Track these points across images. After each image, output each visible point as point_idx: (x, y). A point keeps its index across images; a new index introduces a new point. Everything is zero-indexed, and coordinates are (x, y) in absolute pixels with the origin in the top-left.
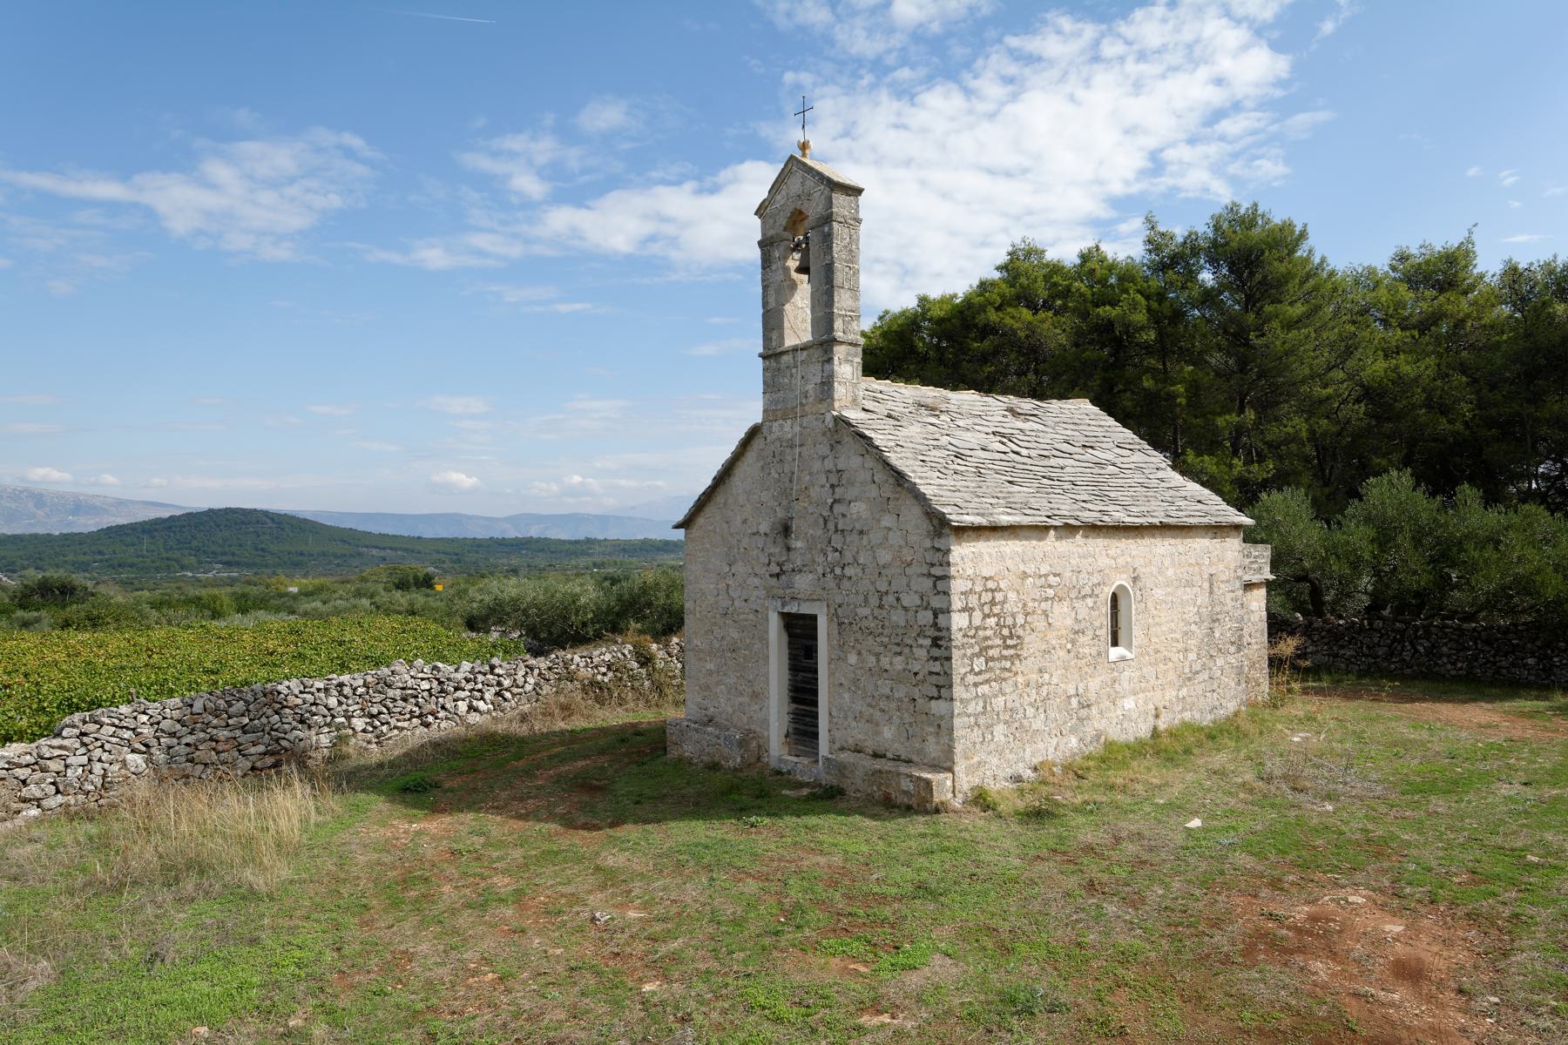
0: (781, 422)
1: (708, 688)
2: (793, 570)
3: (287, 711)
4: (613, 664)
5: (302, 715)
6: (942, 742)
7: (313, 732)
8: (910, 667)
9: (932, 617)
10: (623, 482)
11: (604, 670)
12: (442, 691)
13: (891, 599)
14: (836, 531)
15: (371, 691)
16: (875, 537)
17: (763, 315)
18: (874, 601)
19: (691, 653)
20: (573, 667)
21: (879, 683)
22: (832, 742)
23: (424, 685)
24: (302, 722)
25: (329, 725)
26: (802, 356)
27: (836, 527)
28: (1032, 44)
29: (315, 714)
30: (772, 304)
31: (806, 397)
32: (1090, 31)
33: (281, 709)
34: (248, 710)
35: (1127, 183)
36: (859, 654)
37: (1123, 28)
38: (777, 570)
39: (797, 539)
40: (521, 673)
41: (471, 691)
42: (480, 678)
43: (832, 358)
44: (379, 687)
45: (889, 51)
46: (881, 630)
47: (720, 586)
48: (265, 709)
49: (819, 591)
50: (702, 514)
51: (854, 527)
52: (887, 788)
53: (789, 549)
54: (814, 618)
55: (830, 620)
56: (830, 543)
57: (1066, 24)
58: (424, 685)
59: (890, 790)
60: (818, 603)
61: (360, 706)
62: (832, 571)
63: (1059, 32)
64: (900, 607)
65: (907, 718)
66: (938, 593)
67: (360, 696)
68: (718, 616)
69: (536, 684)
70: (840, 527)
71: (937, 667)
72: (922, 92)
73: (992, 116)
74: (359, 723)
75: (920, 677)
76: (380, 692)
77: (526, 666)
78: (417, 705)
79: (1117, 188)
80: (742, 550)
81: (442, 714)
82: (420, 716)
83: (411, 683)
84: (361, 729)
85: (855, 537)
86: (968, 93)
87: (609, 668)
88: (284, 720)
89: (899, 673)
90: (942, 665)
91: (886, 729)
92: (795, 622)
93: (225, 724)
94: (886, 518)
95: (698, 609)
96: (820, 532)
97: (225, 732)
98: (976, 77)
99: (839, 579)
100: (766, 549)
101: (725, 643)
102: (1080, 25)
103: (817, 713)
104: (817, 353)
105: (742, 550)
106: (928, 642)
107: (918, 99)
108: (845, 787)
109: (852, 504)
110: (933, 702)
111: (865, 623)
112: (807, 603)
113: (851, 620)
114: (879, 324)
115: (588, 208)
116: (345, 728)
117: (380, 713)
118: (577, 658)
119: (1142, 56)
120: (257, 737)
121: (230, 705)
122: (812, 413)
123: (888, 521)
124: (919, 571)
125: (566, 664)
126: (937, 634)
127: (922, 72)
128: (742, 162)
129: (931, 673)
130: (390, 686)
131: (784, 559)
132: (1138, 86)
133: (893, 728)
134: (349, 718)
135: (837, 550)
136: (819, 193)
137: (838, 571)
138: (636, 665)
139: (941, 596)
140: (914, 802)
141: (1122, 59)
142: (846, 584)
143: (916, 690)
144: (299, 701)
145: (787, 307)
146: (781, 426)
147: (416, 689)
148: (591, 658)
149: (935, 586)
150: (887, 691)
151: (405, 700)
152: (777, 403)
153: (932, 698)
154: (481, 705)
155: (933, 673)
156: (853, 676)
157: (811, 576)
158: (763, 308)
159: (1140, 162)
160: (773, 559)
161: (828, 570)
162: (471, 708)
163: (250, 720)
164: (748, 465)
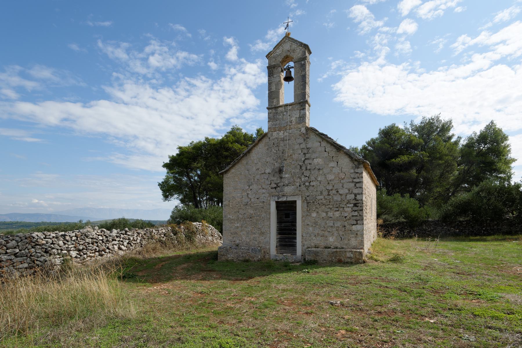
0: (278, 132)
2: (284, 185)
3: (38, 247)
4: (166, 234)
5: (46, 249)
6: (358, 239)
7: (52, 257)
8: (343, 215)
10: (55, 203)
11: (163, 236)
12: (107, 241)
13: (334, 192)
14: (306, 169)
15: (79, 239)
16: (325, 171)
23: (101, 238)
24: (46, 252)
25: (58, 254)
28: (194, 82)
29: (53, 249)
31: (291, 122)
32: (210, 82)
33: (35, 245)
34: (18, 246)
35: (220, 126)
36: (318, 212)
38: (275, 186)
39: (285, 174)
40: (136, 235)
41: (119, 241)
42: (122, 236)
43: (305, 108)
44: (82, 237)
45: (149, 73)
46: (328, 203)
47: (243, 194)
48: (27, 245)
49: (297, 192)
50: (234, 168)
51: (316, 168)
53: (281, 178)
54: (295, 202)
55: (303, 202)
57: (204, 78)
58: (101, 238)
59: (342, 258)
60: (297, 196)
61: (74, 246)
62: (304, 184)
63: (201, 80)
64: (338, 194)
65: (341, 233)
66: (357, 188)
67: (74, 241)
69: (141, 240)
70: (308, 168)
71: (356, 214)
72: (160, 89)
74: (74, 254)
75: (348, 217)
76: (83, 240)
77: (137, 233)
78: (97, 246)
79: (218, 127)
81: (107, 251)
82: (99, 251)
83: (95, 236)
84: (74, 256)
85: (316, 171)
86: (175, 92)
87: (164, 235)
88: (37, 251)
89: (337, 217)
91: (330, 238)
93: (4, 252)
94: (332, 163)
95: (231, 204)
96: (298, 171)
97: (6, 257)
99: (307, 187)
101: (246, 215)
103: (296, 237)
104: (298, 106)
105: (256, 180)
106: (352, 205)
107: (159, 90)
108: (318, 259)
110: (353, 226)
111: (320, 201)
114: (190, 145)
115: (38, 105)
116: (66, 256)
117: (83, 249)
118: (154, 231)
120: (24, 259)
121: (8, 243)
122: (294, 128)
124: (348, 181)
126: (356, 202)
128: (100, 100)
129: (353, 216)
130: (87, 237)
131: (279, 181)
133: (334, 237)
134: (69, 251)
135: (307, 176)
136: (299, 50)
137: (307, 184)
138: (172, 235)
139: (359, 189)
140: (353, 260)
141: (219, 90)
142: (311, 188)
143: (346, 223)
144: (44, 242)
146: (278, 134)
147: (97, 239)
150: (332, 224)
151: (93, 244)
154: (122, 247)
156: (314, 221)
157: (293, 187)
158: (269, 90)
159: (223, 121)
161: (302, 184)
162: (120, 249)
163: (20, 250)
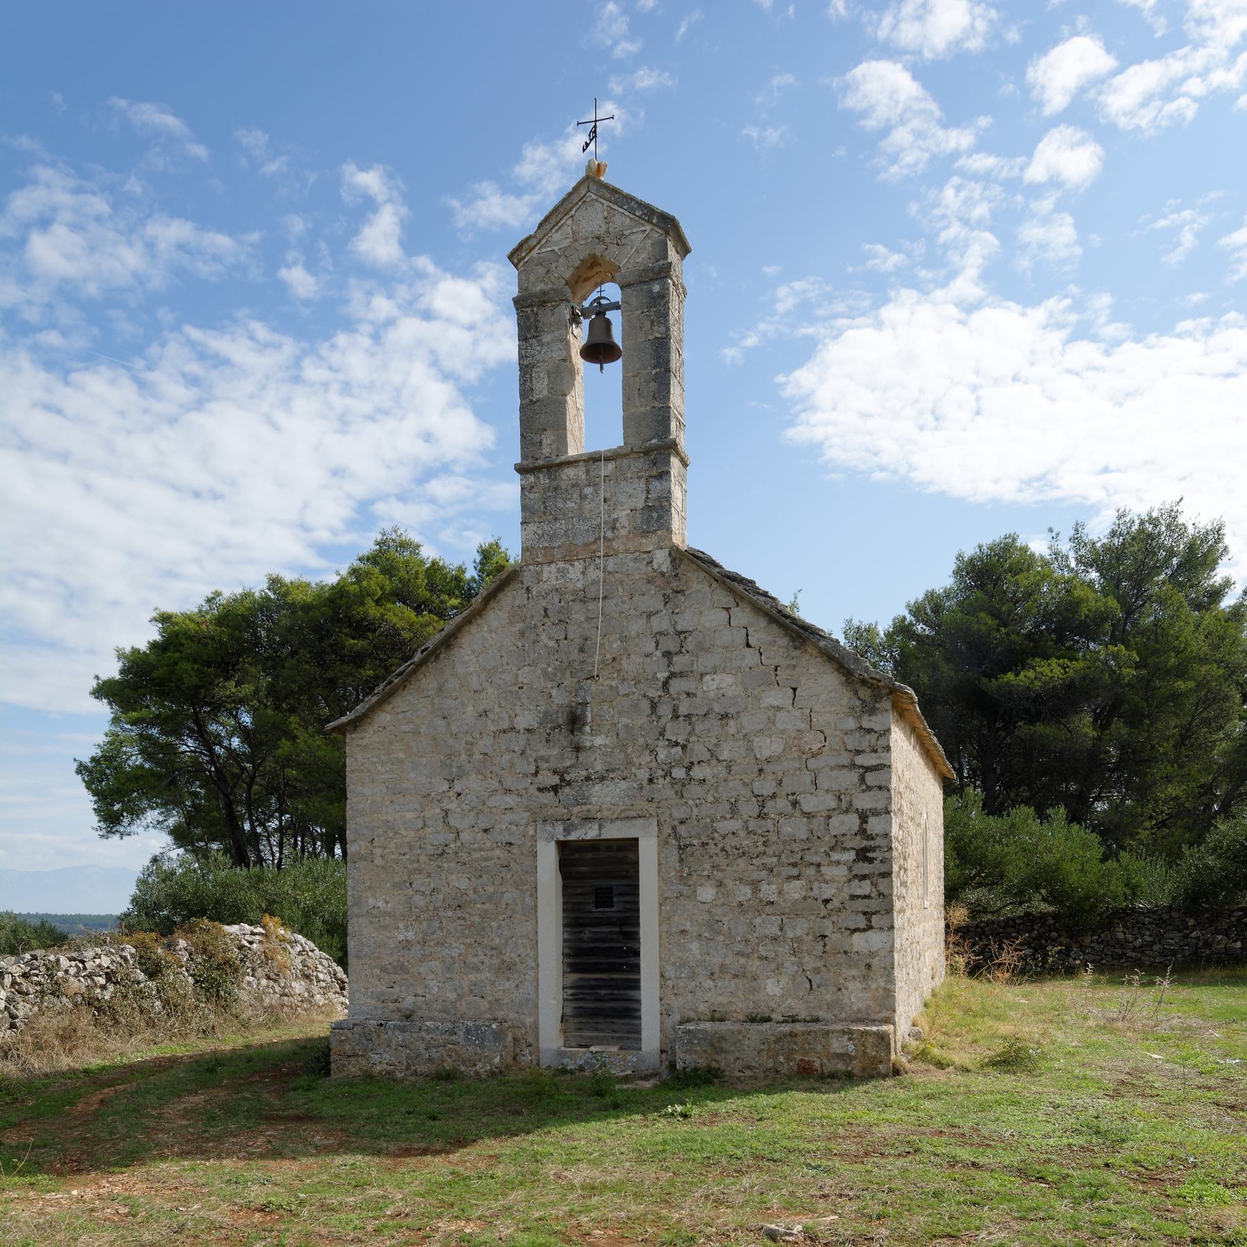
0: (561, 565)
1: (401, 968)
2: (588, 778)
4: (114, 973)
6: (874, 986)
8: (815, 892)
9: (858, 822)
13: (782, 804)
16: (749, 722)
17: (522, 408)
18: (749, 809)
19: (361, 920)
20: (60, 974)
21: (758, 920)
22: (666, 1013)
26: (607, 469)
27: (675, 710)
28: (221, 345)
30: (542, 388)
31: (614, 529)
32: (289, 347)
35: (334, 532)
36: (720, 884)
37: (324, 349)
46: (761, 849)
47: (428, 814)
50: (388, 708)
51: (711, 709)
52: (806, 1054)
53: (578, 749)
55: (663, 843)
56: (662, 734)
57: (261, 330)
60: (641, 821)
62: (668, 774)
63: (252, 338)
64: (797, 813)
65: (809, 962)
66: (869, 788)
68: (423, 858)
71: (865, 888)
72: (79, 370)
73: (173, 421)
75: (835, 903)
79: (323, 535)
80: (477, 756)
85: (714, 724)
89: (795, 902)
90: (874, 884)
91: (770, 982)
92: (577, 856)
94: (772, 693)
95: (378, 851)
96: (642, 720)
98: (150, 368)
99: (681, 787)
100: (529, 752)
101: (441, 897)
102: (276, 337)
103: (638, 981)
104: (639, 465)
105: (477, 756)
106: (851, 855)
107: (75, 377)
109: (707, 678)
110: (856, 936)
111: (730, 842)
112: (618, 822)
113: (704, 839)
114: (206, 607)
118: (64, 963)
119: (347, 388)
122: (627, 551)
123: (776, 697)
124: (833, 762)
125: (51, 969)
126: (865, 843)
127: (79, 343)
129: (853, 897)
131: (568, 763)
132: (344, 422)
133: (784, 980)
135: (677, 744)
136: (641, 236)
137: (679, 773)
138: (141, 976)
140: (856, 1067)
141: (326, 385)
142: (694, 790)
143: (828, 923)
145: (568, 398)
146: (563, 572)
148: (83, 962)
149: (862, 780)
150: (774, 930)
152: (552, 538)
153: (856, 930)
155: (858, 897)
156: (706, 917)
157: (623, 785)
159: (345, 511)
160: (543, 765)
164: (490, 631)
